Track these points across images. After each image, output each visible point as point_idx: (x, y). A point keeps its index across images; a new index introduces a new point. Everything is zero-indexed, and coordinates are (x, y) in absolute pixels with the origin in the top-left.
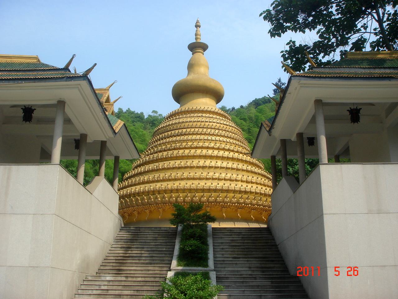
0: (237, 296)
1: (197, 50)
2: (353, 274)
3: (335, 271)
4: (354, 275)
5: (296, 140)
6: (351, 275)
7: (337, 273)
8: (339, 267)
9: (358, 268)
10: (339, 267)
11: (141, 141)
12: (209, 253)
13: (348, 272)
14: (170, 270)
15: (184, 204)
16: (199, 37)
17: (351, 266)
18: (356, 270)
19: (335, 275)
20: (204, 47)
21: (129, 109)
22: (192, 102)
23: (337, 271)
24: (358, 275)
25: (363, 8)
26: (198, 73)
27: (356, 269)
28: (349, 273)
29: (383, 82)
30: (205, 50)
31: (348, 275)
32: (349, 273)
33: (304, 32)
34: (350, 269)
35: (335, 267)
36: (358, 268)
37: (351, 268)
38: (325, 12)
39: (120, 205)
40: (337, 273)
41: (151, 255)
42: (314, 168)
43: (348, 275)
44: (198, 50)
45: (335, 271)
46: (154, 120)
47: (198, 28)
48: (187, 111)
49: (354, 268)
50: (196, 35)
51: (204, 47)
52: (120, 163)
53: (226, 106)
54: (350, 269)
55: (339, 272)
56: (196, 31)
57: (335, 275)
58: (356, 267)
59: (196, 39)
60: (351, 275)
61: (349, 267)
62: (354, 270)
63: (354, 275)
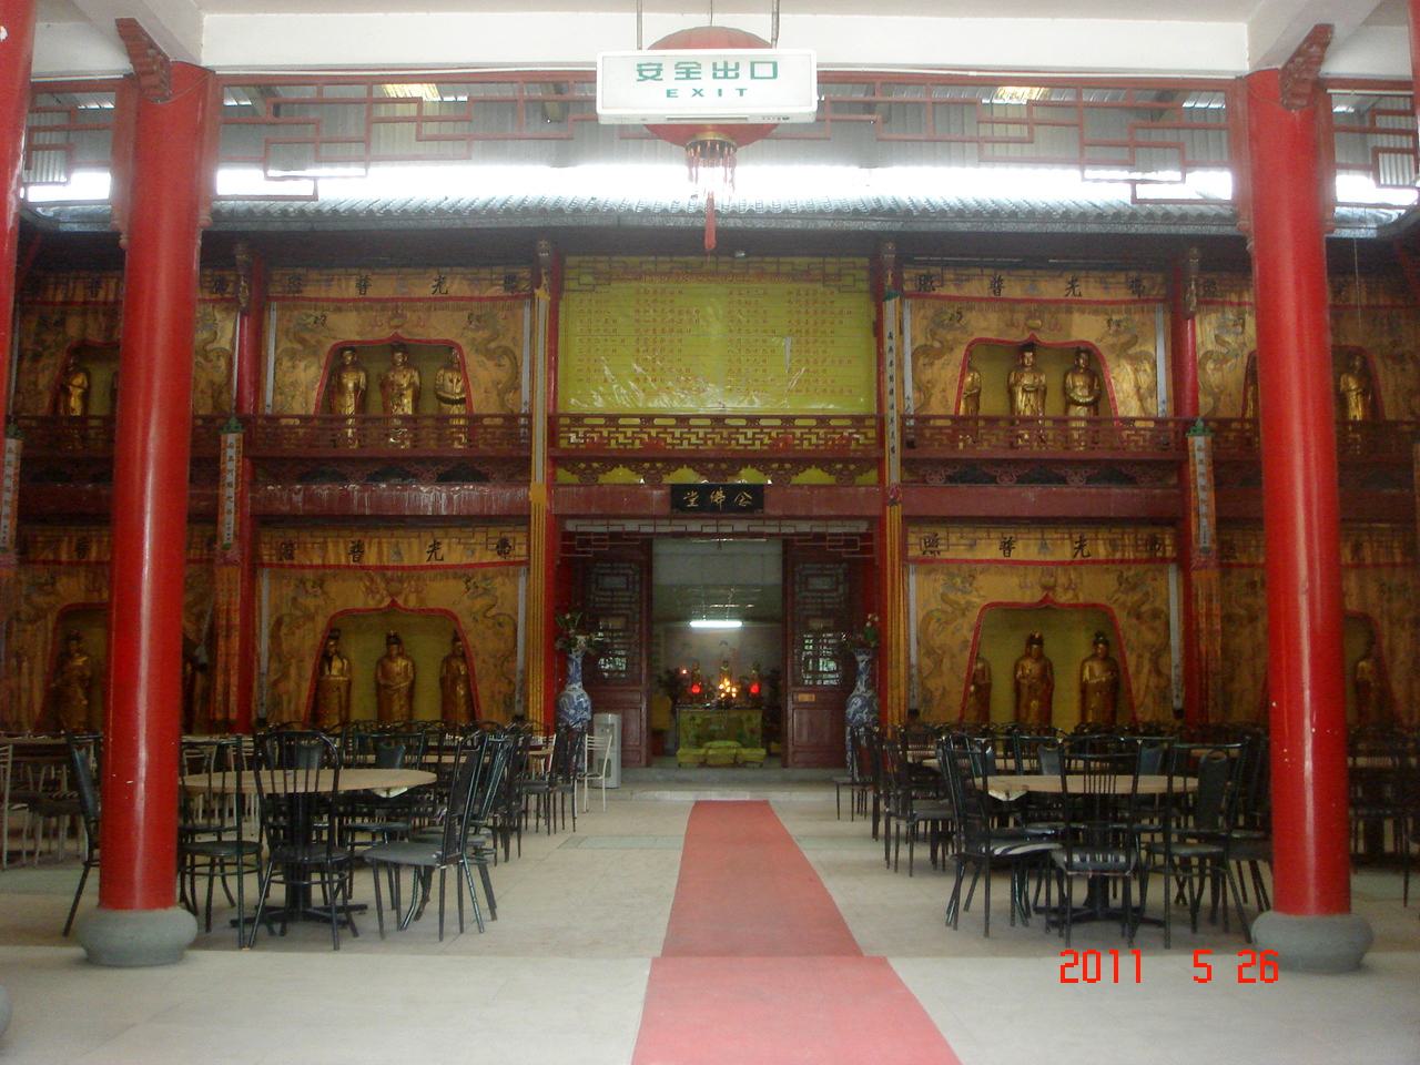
0: (1395, 99)
2: (1081, 977)
3: (1197, 964)
4: (1085, 978)
5: (209, 19)
6: (1075, 981)
12: (964, 166)
14: (228, 419)
19: (1196, 978)
24: (1098, 978)
28: (1069, 973)
31: (1064, 980)
38: (1389, 812)
40: (1202, 972)
41: (559, 815)
43: (1064, 980)
45: (1197, 964)
55: (1209, 968)
57: (1196, 978)
60: (1075, 981)
63: (1085, 978)
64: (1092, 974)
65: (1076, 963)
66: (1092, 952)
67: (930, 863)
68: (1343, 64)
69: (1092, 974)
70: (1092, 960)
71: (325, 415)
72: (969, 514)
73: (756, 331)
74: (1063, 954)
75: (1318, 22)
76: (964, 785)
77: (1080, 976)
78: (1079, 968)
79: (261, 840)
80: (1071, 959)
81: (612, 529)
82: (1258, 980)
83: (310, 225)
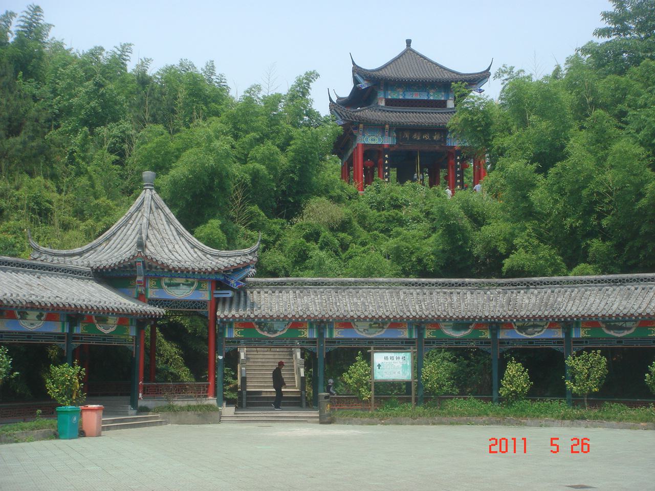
1: (124, 318)
2: (498, 450)
3: (552, 445)
7: (555, 448)
8: (558, 439)
9: (589, 440)
10: (558, 439)
11: (401, 222)
13: (572, 446)
15: (420, 335)
17: (578, 438)
18: (586, 444)
19: (552, 451)
24: (507, 451)
25: (386, 156)
27: (585, 441)
31: (491, 452)
32: (575, 449)
34: (575, 442)
35: (552, 439)
36: (589, 440)
37: (578, 440)
40: (555, 448)
43: (491, 452)
45: (552, 445)
49: (582, 440)
52: (503, 209)
54: (575, 442)
55: (558, 446)
57: (552, 451)
58: (555, 439)
60: (496, 452)
61: (494, 439)
62: (583, 444)
63: (582, 451)
64: (504, 449)
69: (504, 449)
73: (195, 396)
75: (39, 5)
76: (359, 349)
77: (498, 450)
78: (498, 446)
79: (241, 368)
81: (139, 197)
83: (93, 284)
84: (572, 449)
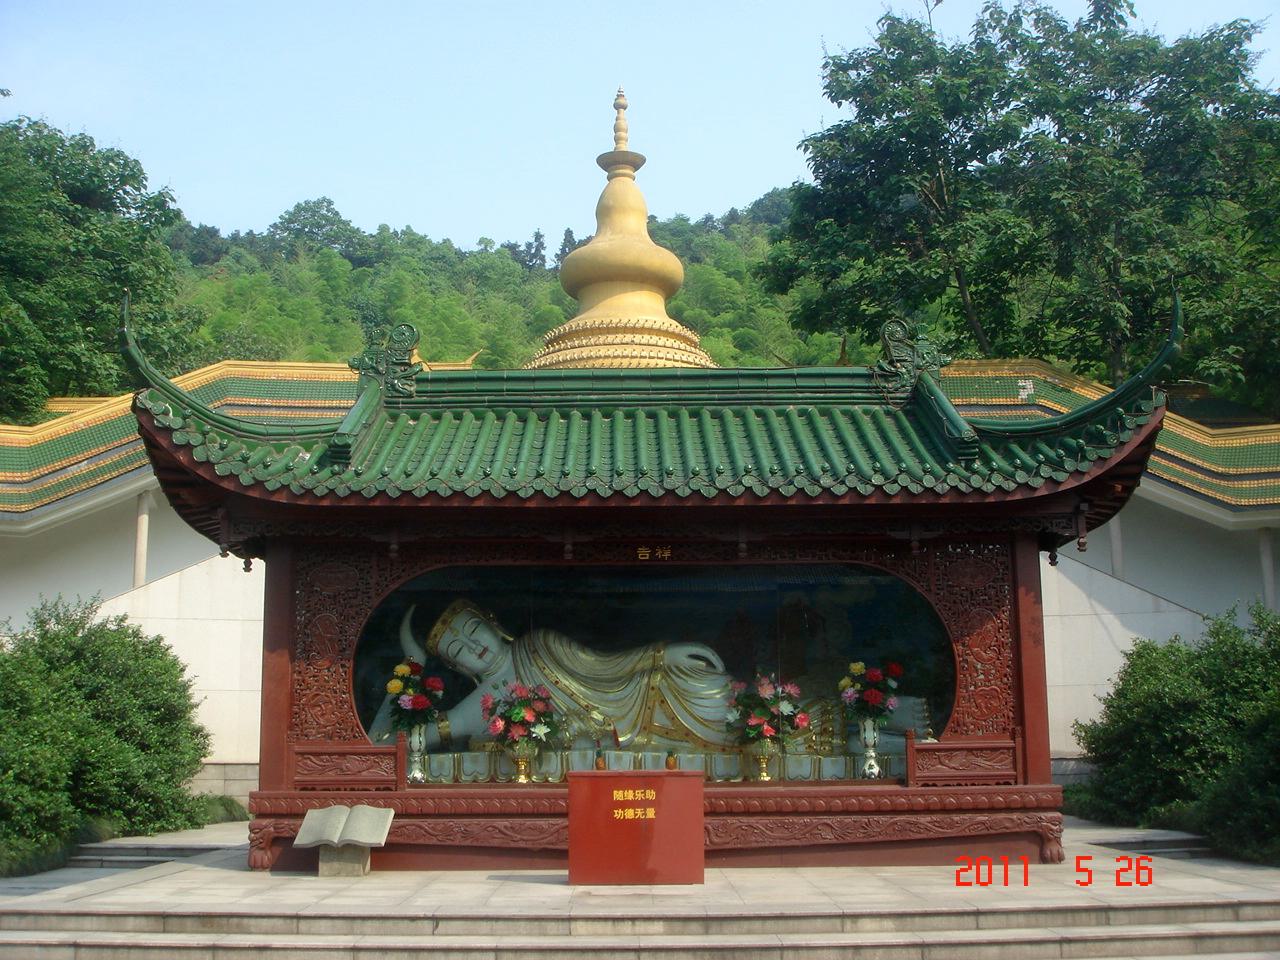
1: (622, 168)
3: (1079, 869)
4: (978, 882)
6: (1130, 884)
7: (1084, 877)
10: (1090, 858)
13: (1118, 873)
16: (623, 134)
18: (1145, 868)
19: (1078, 882)
20: (636, 162)
21: (408, 227)
22: (605, 302)
23: (1085, 870)
26: (621, 232)
28: (1124, 877)
29: (148, 942)
30: (636, 167)
31: (1119, 883)
32: (1124, 877)
33: (840, 105)
35: (1079, 859)
39: (1208, 420)
40: (1084, 877)
42: (946, 423)
43: (1119, 883)
44: (621, 171)
45: (1079, 869)
46: (485, 268)
47: (622, 110)
48: (599, 328)
50: (617, 129)
51: (636, 162)
53: (687, 214)
56: (617, 119)
57: (1078, 882)
59: (617, 140)
60: (1130, 884)
62: (1139, 868)
63: (978, 882)
64: (984, 878)
65: (970, 868)
66: (984, 858)
67: (618, 733)
68: (108, 626)
69: (984, 878)
70: (984, 868)
71: (1166, 353)
72: (1025, 700)
74: (1118, 860)
80: (1124, 864)
82: (1134, 883)
84: (958, 878)
